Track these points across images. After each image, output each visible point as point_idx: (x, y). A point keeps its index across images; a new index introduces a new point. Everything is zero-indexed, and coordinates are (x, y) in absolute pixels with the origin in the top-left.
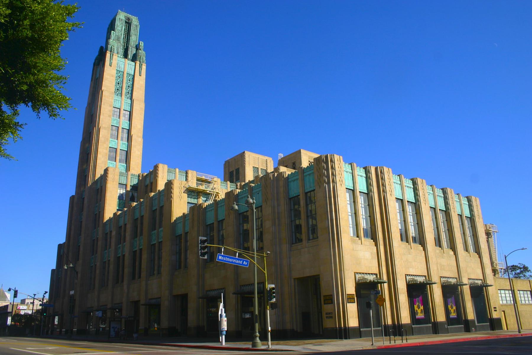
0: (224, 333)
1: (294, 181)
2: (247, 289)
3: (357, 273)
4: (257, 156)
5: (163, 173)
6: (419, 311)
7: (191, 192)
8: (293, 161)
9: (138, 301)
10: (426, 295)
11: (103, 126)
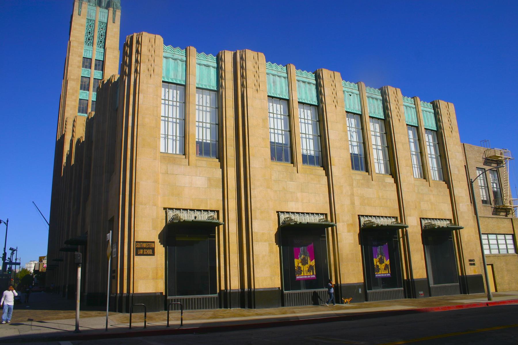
3: (423, 218)
6: (382, 267)
11: (72, 77)
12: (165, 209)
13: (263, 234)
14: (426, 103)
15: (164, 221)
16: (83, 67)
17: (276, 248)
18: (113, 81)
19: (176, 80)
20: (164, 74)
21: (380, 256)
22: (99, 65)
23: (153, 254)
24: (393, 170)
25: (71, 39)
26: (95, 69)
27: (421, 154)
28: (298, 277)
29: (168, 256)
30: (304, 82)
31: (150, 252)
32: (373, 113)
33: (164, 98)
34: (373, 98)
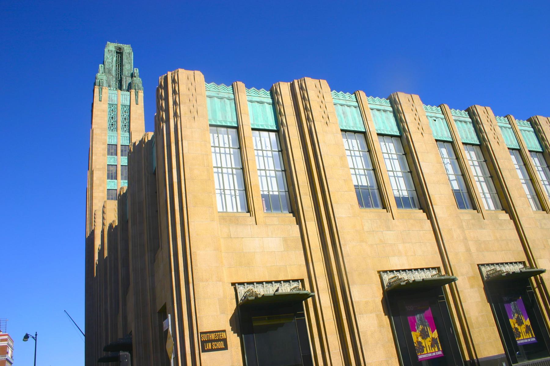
6: (522, 329)
11: (97, 167)
12: (233, 284)
13: (367, 303)
14: (521, 122)
15: (234, 301)
16: (108, 154)
17: (386, 320)
18: (146, 141)
19: (225, 121)
20: (210, 117)
21: (516, 315)
22: (125, 150)
23: (226, 348)
24: (505, 204)
25: (93, 127)
26: (122, 155)
28: (420, 357)
29: (246, 349)
31: (221, 345)
32: (465, 138)
33: (213, 145)
34: (461, 121)
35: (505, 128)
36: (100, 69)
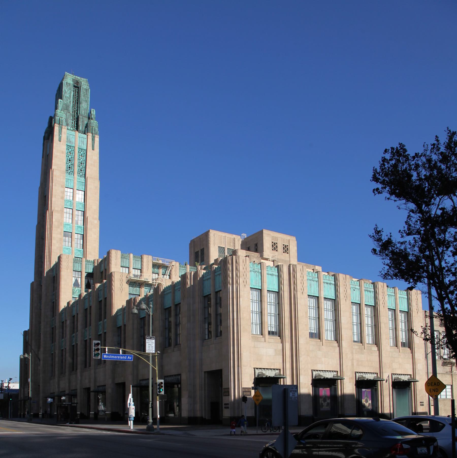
0: (132, 419)
1: (207, 279)
2: (144, 383)
4: (223, 234)
5: (116, 259)
6: (325, 404)
7: (132, 283)
8: (255, 243)
9: (89, 389)
10: (376, 390)
11: (56, 209)
13: (305, 384)
27: (396, 329)
30: (327, 283)
34: (368, 291)
35: (391, 295)
36: (60, 105)
